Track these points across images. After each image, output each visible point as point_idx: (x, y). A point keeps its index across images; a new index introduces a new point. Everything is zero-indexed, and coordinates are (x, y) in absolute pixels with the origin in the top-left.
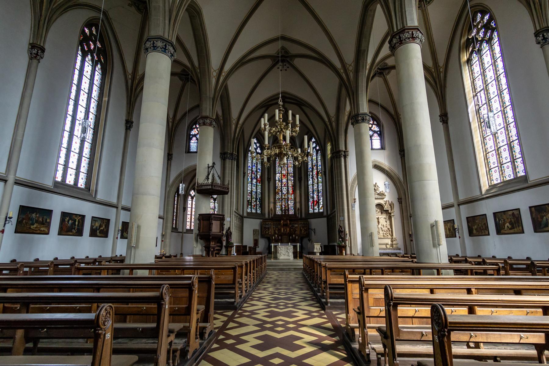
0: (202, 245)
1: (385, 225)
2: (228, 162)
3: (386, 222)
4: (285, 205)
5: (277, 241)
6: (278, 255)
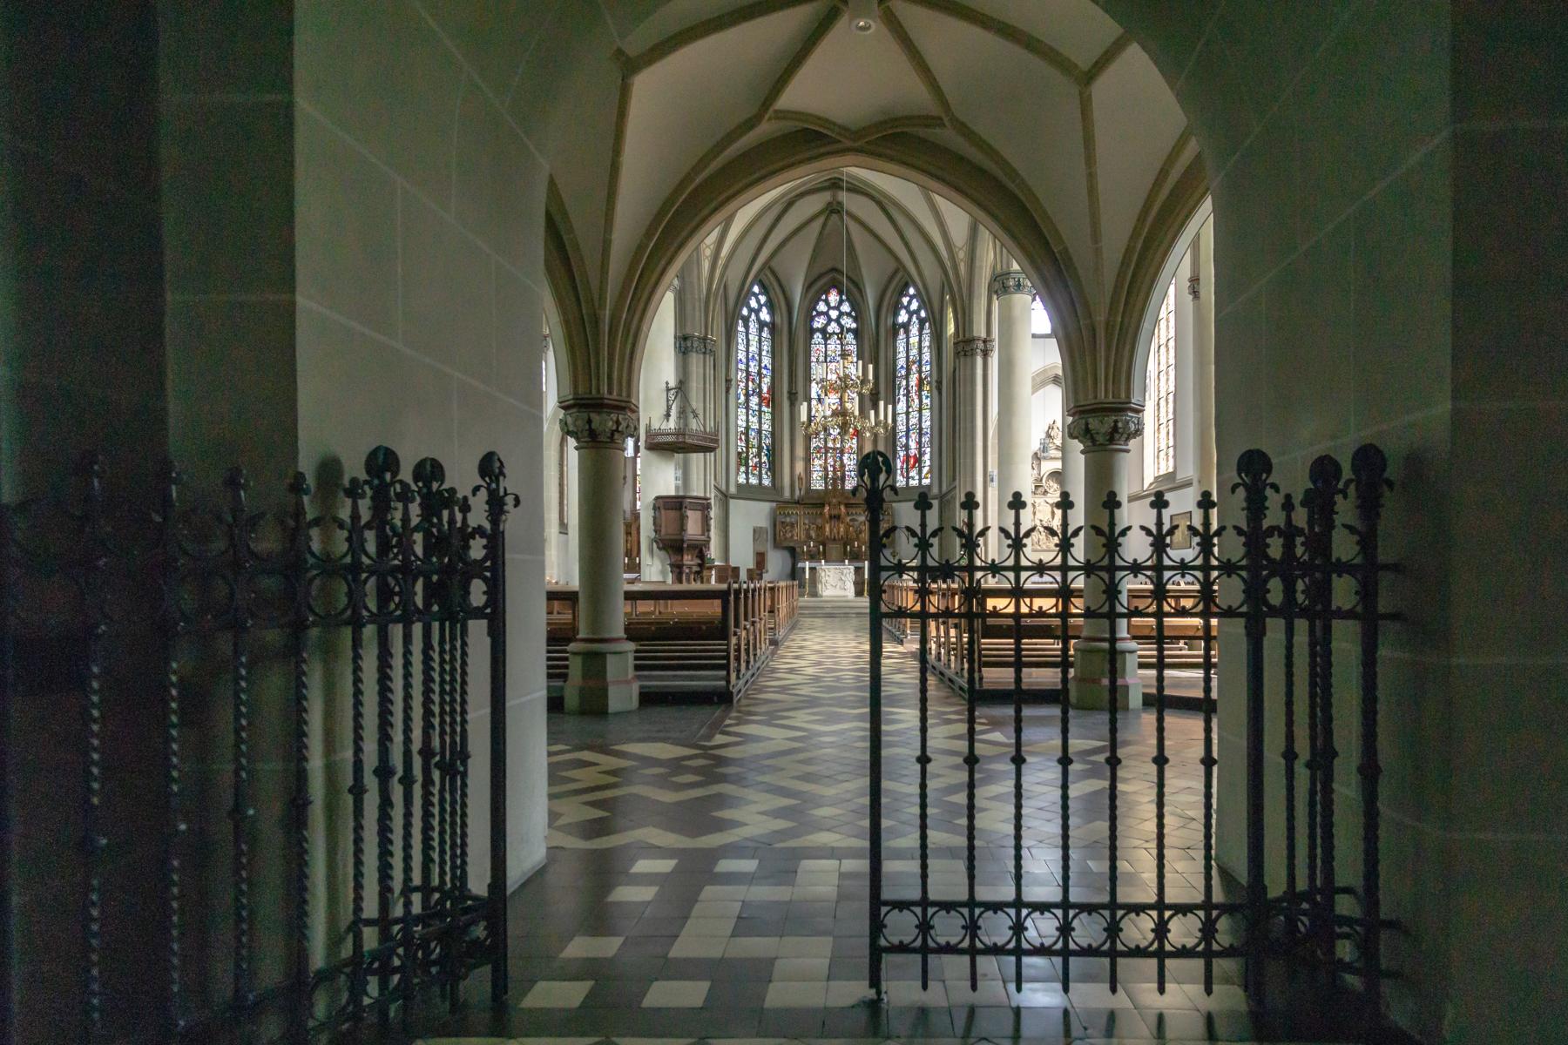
0: (662, 562)
2: (695, 360)
4: (834, 466)
5: (813, 557)
6: (820, 587)
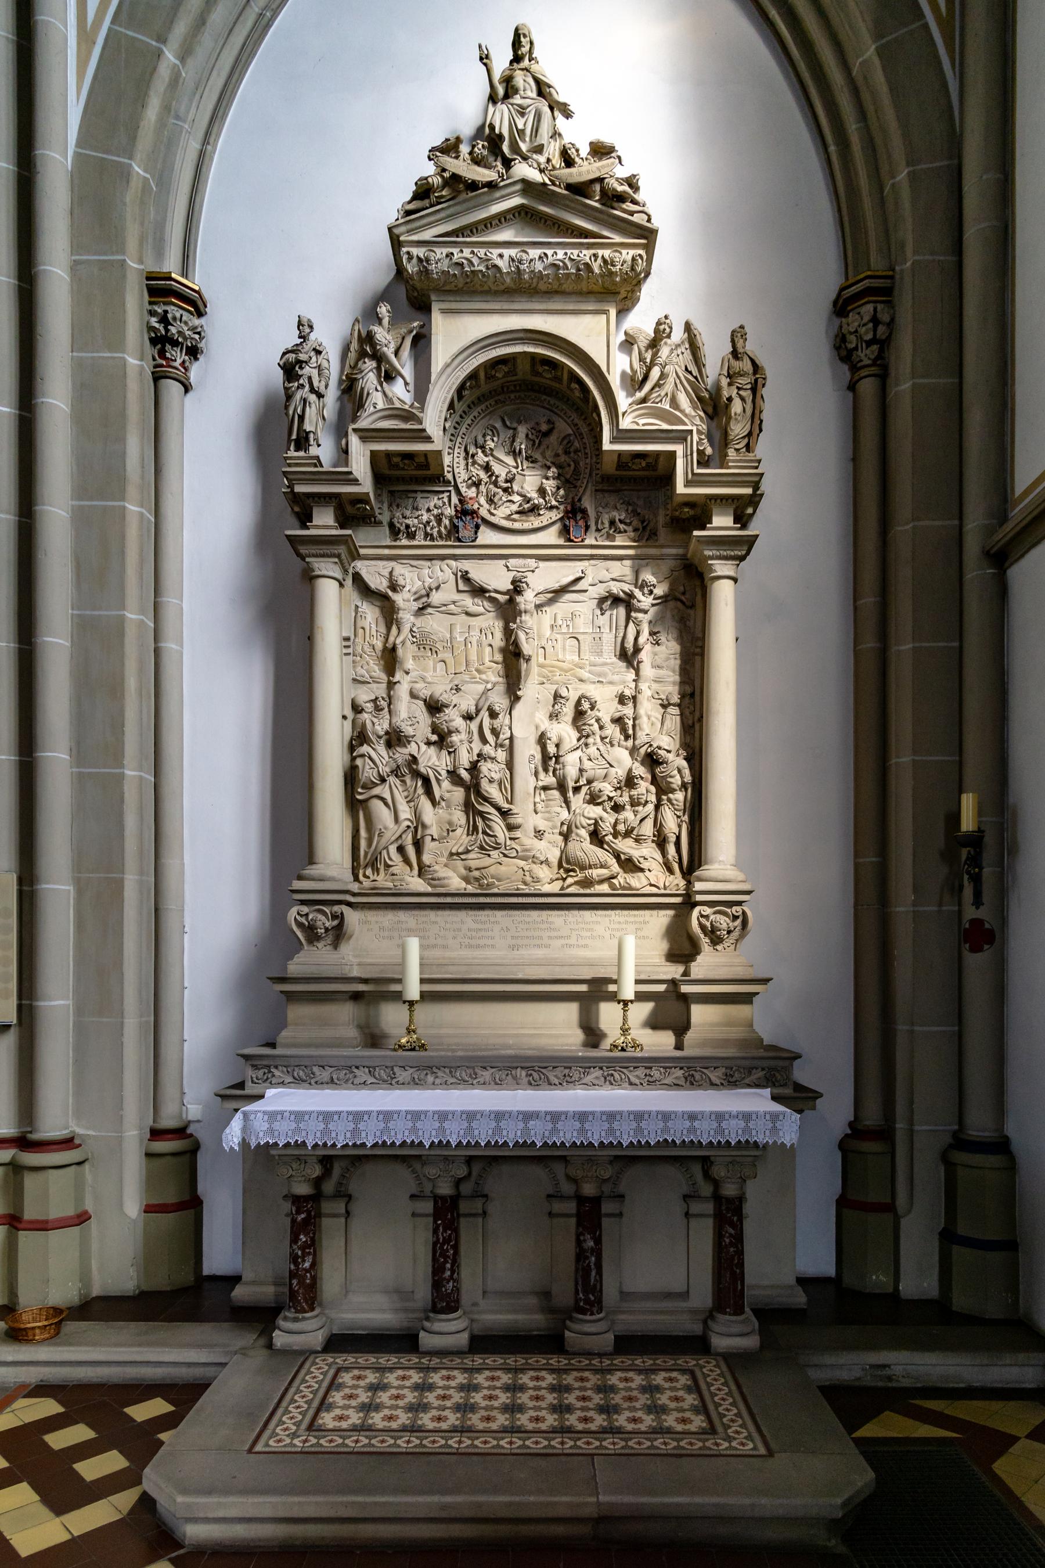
1: (607, 709)
3: (629, 656)
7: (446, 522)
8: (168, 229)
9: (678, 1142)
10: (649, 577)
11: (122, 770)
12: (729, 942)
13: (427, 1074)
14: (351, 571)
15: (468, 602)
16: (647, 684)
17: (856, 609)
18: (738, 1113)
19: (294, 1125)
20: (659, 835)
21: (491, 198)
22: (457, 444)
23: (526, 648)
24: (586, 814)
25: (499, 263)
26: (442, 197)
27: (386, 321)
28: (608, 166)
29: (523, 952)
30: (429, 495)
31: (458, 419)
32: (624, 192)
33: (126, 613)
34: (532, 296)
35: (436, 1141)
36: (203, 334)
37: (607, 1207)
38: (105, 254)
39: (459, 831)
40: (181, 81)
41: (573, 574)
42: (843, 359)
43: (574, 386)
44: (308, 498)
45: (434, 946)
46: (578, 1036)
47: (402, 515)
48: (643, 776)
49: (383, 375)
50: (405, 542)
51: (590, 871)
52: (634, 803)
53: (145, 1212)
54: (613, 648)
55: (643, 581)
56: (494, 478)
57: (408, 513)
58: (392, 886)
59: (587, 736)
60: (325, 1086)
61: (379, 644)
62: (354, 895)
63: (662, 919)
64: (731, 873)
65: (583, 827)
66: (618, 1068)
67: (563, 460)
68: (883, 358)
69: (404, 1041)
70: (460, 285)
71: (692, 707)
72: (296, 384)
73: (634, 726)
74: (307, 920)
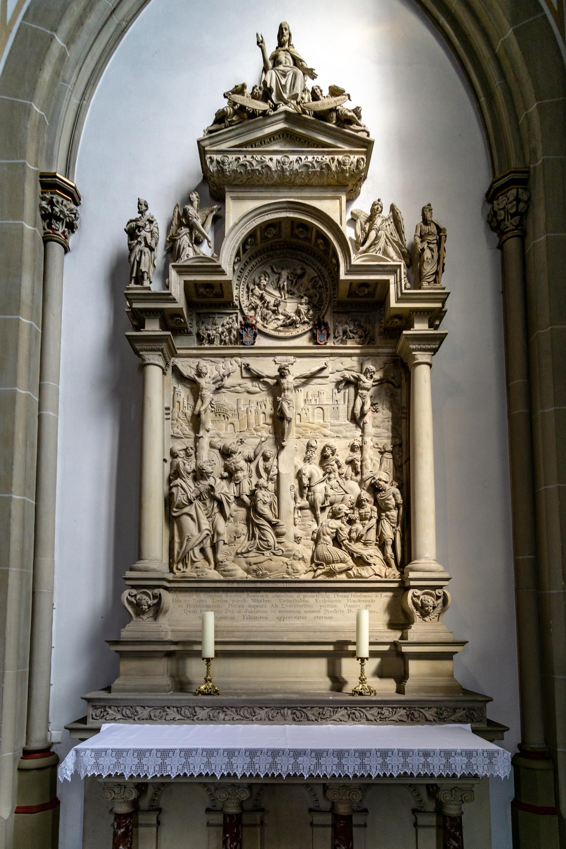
1: (343, 455)
7: (235, 332)
8: (56, 147)
9: (415, 775)
10: (372, 367)
11: (10, 495)
12: (434, 615)
13: (219, 713)
14: (171, 364)
15: (249, 385)
16: (370, 438)
17: (508, 388)
18: (462, 751)
19: (114, 760)
20: (380, 541)
21: (264, 123)
22: (242, 283)
23: (289, 413)
24: (330, 525)
25: (270, 164)
26: (233, 121)
27: (196, 203)
28: (341, 100)
29: (287, 622)
30: (223, 316)
31: (242, 266)
32: (352, 117)
33: (17, 389)
34: (291, 188)
35: (226, 773)
36: (77, 216)
37: (357, 819)
38: (13, 159)
39: (243, 538)
40: (67, 59)
41: (319, 365)
42: (493, 229)
43: (320, 241)
44: (142, 312)
45: (225, 618)
46: (327, 683)
47: (206, 328)
48: (368, 499)
49: (193, 239)
50: (207, 346)
51: (333, 565)
52: (363, 518)
53: (16, 812)
54: (346, 415)
55: (367, 369)
56: (266, 305)
57: (210, 327)
58: (196, 576)
59: (330, 473)
60: (145, 721)
61: (189, 413)
62: (170, 581)
63: (384, 599)
64: (435, 566)
65: (328, 535)
66: (358, 708)
67: (311, 292)
68: (522, 225)
69: (202, 687)
70: (244, 181)
71: (400, 453)
72: (136, 241)
73: (361, 466)
74: (135, 599)
